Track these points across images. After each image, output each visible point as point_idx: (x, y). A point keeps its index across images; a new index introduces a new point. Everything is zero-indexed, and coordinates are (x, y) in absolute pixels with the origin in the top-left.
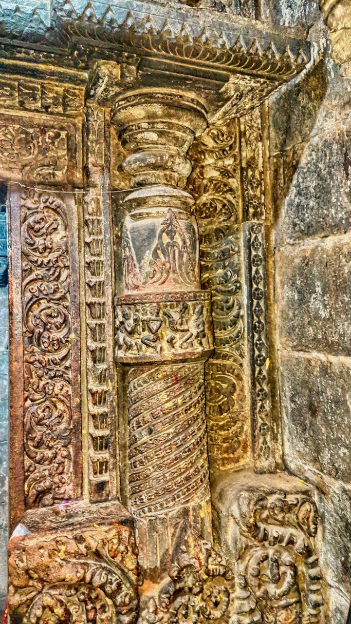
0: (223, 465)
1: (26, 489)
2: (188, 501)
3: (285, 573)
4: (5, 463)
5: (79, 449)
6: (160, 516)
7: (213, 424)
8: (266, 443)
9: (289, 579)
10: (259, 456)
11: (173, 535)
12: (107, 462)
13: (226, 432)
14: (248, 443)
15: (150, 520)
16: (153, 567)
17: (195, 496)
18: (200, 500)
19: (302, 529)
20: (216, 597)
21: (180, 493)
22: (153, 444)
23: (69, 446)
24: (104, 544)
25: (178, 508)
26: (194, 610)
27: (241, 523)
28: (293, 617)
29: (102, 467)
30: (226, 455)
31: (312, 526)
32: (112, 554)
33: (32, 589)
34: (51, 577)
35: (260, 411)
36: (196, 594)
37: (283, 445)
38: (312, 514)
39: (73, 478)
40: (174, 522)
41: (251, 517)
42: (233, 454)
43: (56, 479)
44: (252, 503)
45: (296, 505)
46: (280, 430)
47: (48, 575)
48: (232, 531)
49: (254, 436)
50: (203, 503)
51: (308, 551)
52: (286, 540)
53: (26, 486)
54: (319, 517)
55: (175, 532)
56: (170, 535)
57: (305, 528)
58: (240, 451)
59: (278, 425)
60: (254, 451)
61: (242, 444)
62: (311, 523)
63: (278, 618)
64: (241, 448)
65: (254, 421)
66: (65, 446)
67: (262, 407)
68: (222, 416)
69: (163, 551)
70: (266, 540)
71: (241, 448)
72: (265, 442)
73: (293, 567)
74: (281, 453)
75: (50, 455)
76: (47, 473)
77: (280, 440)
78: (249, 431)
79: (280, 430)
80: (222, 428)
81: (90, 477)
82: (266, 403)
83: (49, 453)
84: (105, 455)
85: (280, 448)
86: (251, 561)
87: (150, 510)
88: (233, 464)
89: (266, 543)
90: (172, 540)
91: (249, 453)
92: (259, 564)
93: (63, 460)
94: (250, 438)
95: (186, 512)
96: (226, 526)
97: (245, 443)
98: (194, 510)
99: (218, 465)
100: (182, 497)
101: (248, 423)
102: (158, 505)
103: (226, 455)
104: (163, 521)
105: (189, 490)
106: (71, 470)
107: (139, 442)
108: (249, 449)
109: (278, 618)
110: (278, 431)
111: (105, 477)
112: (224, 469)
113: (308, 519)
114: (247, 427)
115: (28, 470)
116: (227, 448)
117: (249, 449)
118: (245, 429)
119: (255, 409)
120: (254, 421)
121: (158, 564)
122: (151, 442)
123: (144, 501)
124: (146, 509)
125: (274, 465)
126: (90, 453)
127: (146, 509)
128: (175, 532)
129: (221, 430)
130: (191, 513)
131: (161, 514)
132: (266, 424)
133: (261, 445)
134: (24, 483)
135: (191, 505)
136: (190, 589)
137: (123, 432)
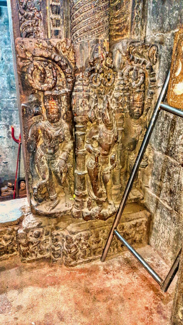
0: (116, 38)
1: (21, 30)
2: (98, 36)
3: (140, 77)
4: (8, 119)
5: (45, 14)
6: (85, 42)
7: (112, 17)
8: (138, 27)
9: (141, 80)
10: (134, 34)
11: (91, 51)
12: (60, 20)
13: (119, 20)
14: (129, 27)
15: (80, 44)
16: (81, 67)
17: (102, 35)
18: (103, 37)
19: (150, 60)
20: (109, 76)
21: (95, 31)
22: (82, 3)
23: (40, 12)
24: (59, 45)
25: (94, 38)
26: (99, 79)
27: (122, 52)
28: (141, 97)
29: (57, 23)
30: (117, 33)
31: (155, 58)
32: (63, 50)
33: (28, 61)
34: (36, 53)
35: (136, 8)
36: (100, 73)
37: (145, 32)
38: (156, 52)
39: (43, 29)
40: (92, 45)
41: (127, 48)
42: (121, 32)
43: (35, 28)
44: (129, 43)
45: (149, 46)
46: (145, 23)
47: (35, 53)
48: (118, 56)
49: (132, 22)
50: (106, 40)
51: (151, 69)
52: (142, 62)
53: (21, 29)
54: (159, 57)
55: (92, 50)
56: (90, 51)
57: (151, 59)
58: (124, 31)
59: (144, 21)
60: (131, 30)
61: (126, 28)
62: (155, 57)
63: (134, 97)
64: (125, 30)
65: (133, 13)
66: (38, 12)
67: (138, 6)
68: (117, 12)
69: (86, 58)
70: (133, 61)
71: (125, 30)
72: (137, 26)
73: (144, 74)
74: (144, 35)
75: (31, 15)
76: (30, 24)
77: (144, 29)
78: (130, 21)
79: (145, 23)
80: (116, 18)
81: (51, 28)
82: (140, 4)
83: (31, 14)
84: (59, 17)
85: (144, 33)
86: (125, 71)
87: (80, 40)
88: (120, 37)
89: (133, 62)
90: (91, 53)
91: (129, 33)
92: (129, 71)
93: (38, 19)
94: (130, 24)
95: (97, 41)
96: (115, 56)
97: (127, 27)
98: (101, 41)
99: (113, 38)
100: (96, 34)
101: (130, 16)
102: (84, 37)
103: (117, 33)
104: (86, 44)
105: (99, 31)
106: (42, 25)
107: (75, 5)
108: (129, 31)
109: (134, 97)
110: (144, 24)
111: (59, 29)
112: (116, 40)
113: (153, 54)
114: (129, 19)
115: (21, 20)
116: (118, 29)
117: (129, 31)
118: (128, 20)
119: (134, 6)
120: (133, 13)
121: (84, 65)
122: (81, 3)
123: (78, 35)
124: (79, 39)
125: (140, 39)
126: (51, 15)
127: (79, 39)
128: (92, 50)
129: (116, 20)
130: (100, 42)
131: (85, 40)
132: (139, 17)
133: (135, 27)
134: (20, 27)
135: (100, 39)
136: (98, 71)
137: (67, 10)
